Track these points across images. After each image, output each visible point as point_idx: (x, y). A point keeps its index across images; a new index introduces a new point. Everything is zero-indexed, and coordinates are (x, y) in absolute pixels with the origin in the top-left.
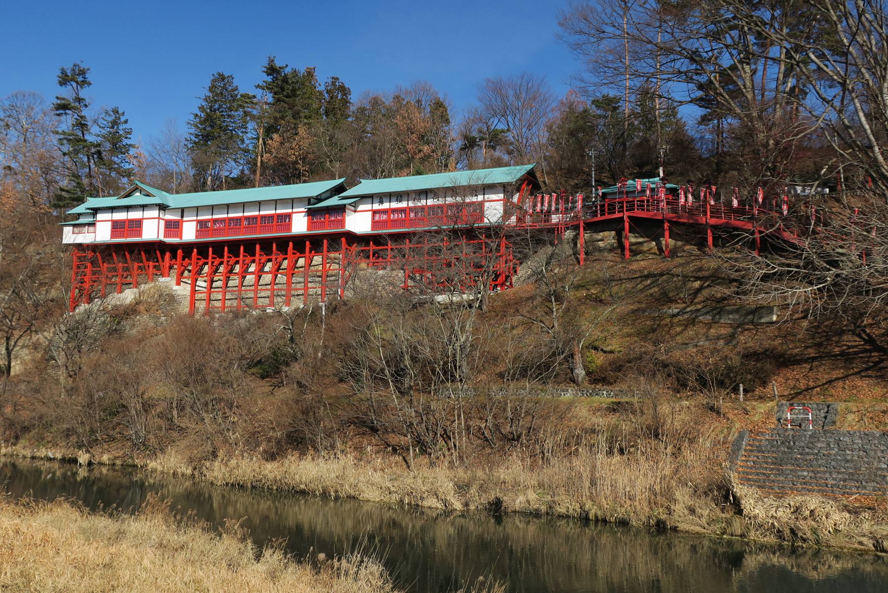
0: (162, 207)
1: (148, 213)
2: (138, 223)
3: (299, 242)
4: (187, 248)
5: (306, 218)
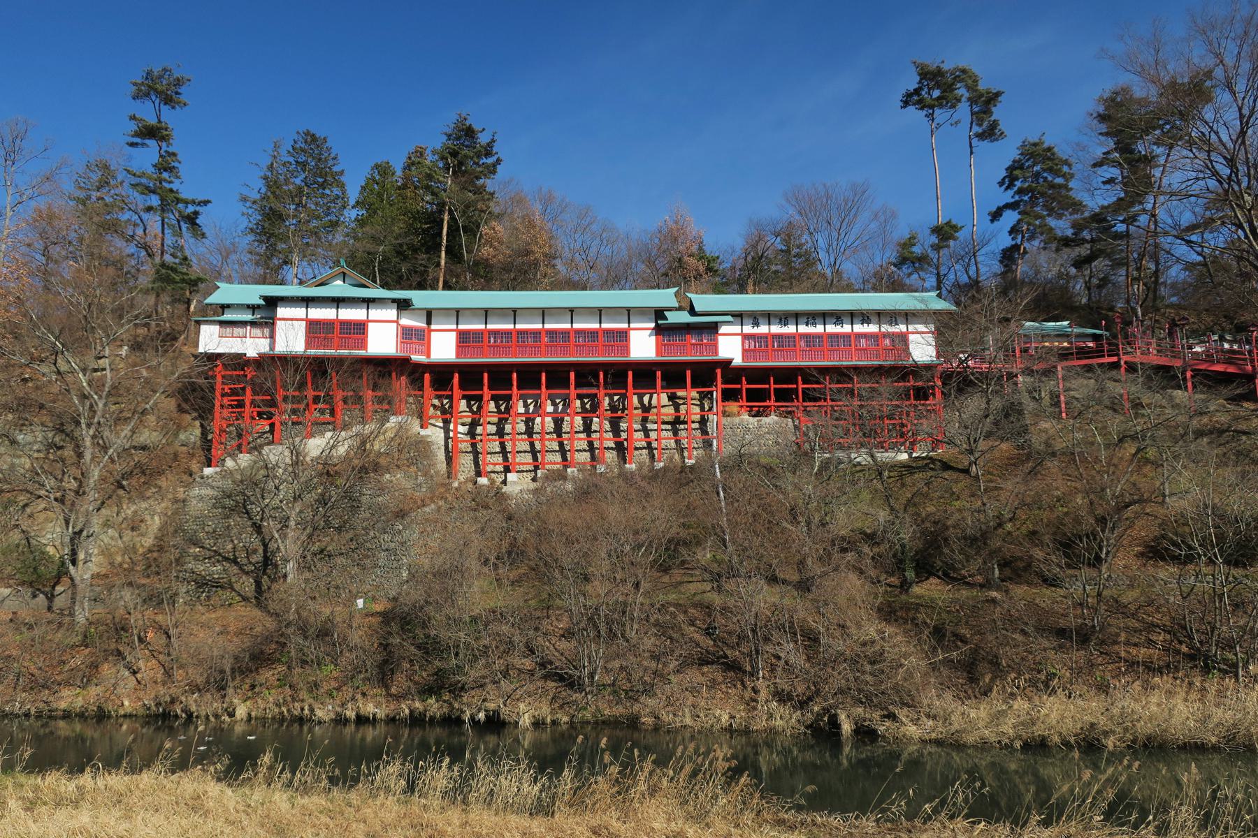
0: (403, 305)
1: (375, 313)
2: (360, 328)
3: (645, 373)
4: (441, 374)
5: (654, 338)
